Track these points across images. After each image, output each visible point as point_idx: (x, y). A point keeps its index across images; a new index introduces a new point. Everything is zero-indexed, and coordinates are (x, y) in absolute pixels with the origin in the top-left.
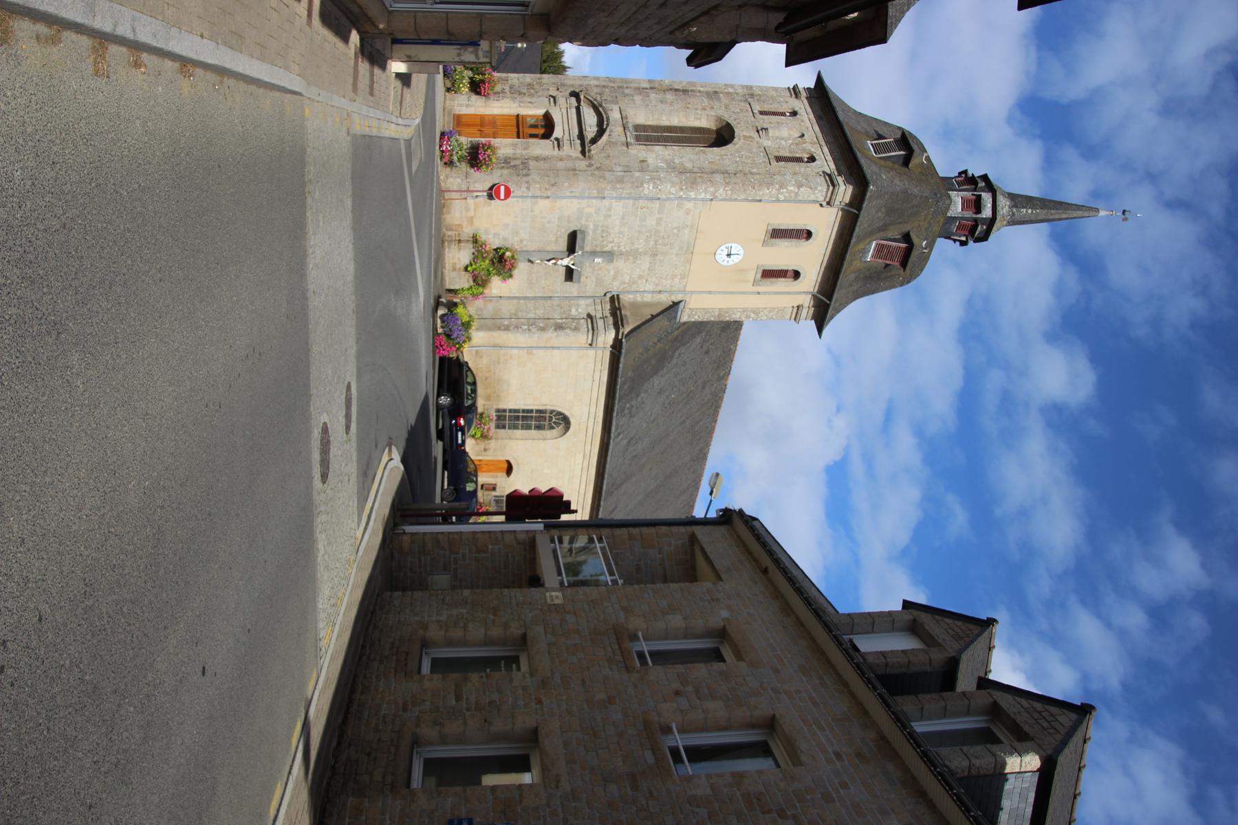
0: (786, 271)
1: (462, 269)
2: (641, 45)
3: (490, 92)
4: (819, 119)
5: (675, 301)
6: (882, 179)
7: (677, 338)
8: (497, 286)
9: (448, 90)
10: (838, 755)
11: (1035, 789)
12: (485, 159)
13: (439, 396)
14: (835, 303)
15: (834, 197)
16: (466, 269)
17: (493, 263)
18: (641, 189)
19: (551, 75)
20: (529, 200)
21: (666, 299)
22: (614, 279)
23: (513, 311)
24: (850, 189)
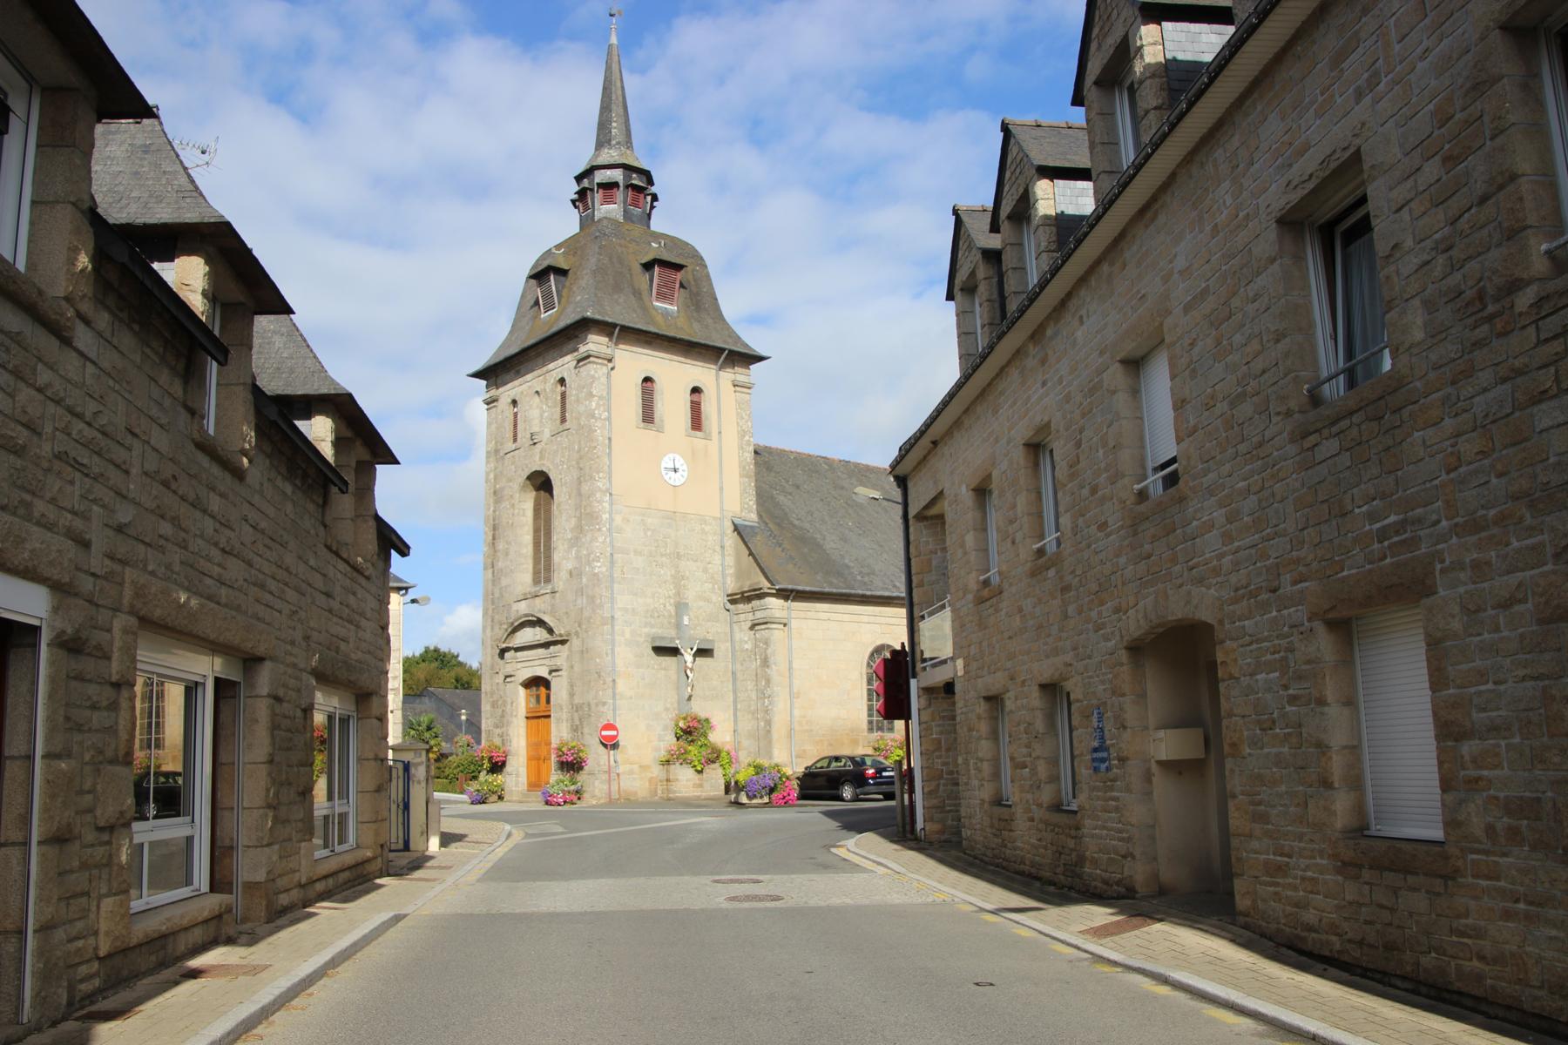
0: (692, 402)
1: (698, 776)
2: (389, 603)
3: (501, 751)
4: (519, 374)
5: (732, 528)
6: (578, 302)
7: (779, 525)
8: (720, 735)
9: (501, 798)
10: (1044, 384)
11: (1072, 182)
12: (572, 754)
13: (842, 800)
14: (728, 344)
15: (602, 355)
16: (700, 772)
17: (692, 741)
18: (601, 576)
19: (483, 682)
20: (618, 702)
21: (731, 540)
22: (709, 601)
23: (750, 716)
24: (592, 337)
